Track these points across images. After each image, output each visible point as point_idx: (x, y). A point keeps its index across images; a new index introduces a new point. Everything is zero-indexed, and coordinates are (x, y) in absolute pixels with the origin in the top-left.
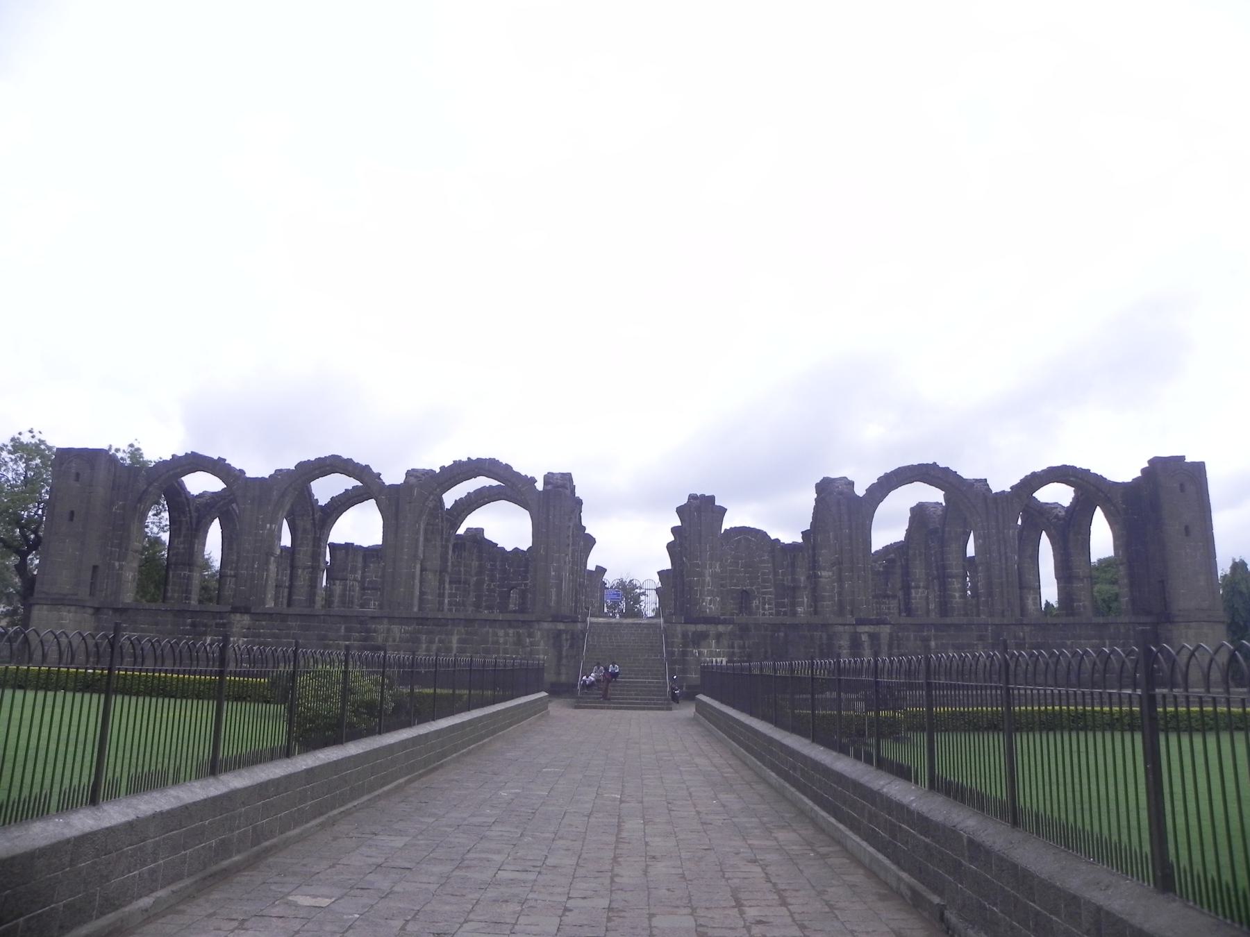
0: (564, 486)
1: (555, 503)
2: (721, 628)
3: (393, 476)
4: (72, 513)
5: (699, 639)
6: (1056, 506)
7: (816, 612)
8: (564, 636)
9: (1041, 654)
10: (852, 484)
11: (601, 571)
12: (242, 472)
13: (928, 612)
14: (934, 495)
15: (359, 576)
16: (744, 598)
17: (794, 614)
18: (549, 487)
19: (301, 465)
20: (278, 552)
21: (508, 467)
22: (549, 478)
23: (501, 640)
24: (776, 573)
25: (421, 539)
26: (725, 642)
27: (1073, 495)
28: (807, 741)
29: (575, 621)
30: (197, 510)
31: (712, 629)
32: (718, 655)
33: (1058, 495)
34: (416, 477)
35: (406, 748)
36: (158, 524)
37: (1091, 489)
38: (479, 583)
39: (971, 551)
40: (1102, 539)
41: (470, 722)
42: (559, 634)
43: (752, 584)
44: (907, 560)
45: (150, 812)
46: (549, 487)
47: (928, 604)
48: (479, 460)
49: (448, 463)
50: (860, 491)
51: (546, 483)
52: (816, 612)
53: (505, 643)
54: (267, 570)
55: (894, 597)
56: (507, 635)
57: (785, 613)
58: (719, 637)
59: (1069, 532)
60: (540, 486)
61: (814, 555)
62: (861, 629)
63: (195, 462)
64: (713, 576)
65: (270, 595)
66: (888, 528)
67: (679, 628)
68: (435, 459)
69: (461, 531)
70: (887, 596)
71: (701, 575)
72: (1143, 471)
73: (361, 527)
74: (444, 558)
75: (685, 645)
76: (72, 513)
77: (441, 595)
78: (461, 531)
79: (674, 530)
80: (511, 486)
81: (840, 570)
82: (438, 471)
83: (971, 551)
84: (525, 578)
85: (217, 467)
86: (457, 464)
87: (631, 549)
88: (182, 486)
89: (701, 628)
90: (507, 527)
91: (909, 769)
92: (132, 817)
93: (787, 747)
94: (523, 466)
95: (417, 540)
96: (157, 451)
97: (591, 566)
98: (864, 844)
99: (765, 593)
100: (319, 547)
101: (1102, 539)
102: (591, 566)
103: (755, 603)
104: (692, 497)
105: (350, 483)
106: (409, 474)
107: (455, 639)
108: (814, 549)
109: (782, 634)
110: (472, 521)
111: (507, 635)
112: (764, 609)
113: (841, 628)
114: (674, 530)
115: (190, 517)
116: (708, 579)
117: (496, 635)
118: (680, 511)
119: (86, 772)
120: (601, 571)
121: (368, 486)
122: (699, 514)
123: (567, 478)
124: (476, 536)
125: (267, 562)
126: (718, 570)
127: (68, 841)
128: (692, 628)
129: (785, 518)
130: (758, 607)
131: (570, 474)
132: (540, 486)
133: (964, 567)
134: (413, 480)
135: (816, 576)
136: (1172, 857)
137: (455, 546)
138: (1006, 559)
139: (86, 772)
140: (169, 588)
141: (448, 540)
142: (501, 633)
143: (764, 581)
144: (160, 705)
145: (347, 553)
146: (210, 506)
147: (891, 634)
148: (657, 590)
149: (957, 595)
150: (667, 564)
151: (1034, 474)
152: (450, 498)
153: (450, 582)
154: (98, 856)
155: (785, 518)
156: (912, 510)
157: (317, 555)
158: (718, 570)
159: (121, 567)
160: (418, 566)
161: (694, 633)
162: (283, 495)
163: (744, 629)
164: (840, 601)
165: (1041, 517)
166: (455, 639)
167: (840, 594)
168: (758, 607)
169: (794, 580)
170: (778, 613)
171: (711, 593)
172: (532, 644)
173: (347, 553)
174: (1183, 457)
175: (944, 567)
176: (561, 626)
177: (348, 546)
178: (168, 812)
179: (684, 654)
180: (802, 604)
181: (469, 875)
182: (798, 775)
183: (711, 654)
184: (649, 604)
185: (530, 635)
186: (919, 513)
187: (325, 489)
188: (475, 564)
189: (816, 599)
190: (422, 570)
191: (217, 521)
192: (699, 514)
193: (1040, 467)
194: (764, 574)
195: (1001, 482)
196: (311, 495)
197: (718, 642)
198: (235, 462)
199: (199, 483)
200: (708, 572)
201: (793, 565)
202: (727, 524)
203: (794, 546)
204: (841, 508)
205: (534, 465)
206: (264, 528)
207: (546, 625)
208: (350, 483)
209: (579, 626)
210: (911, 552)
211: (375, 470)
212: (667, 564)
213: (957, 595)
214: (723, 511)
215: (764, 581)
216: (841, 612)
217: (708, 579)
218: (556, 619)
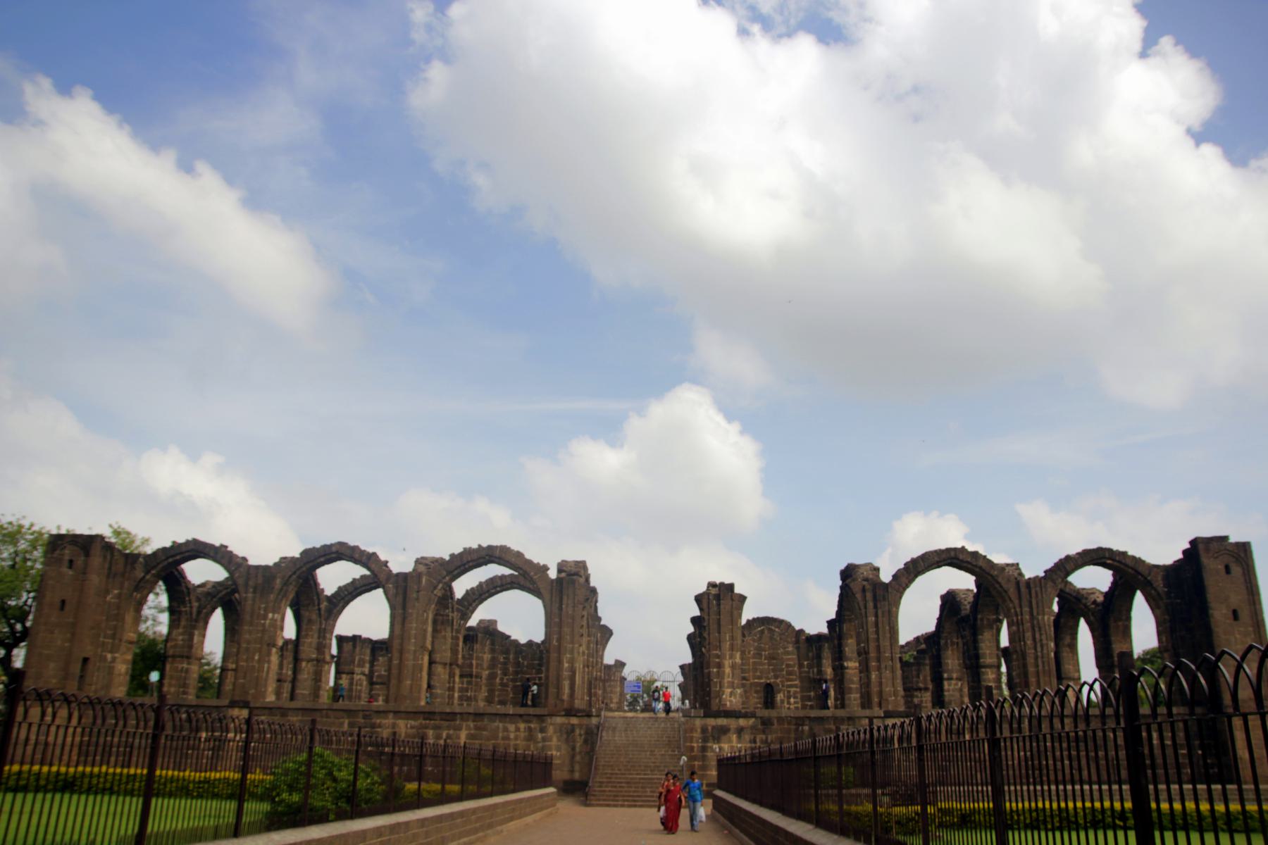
1: (569, 592)
2: (742, 722)
3: (401, 563)
4: (63, 602)
5: (722, 731)
6: (1093, 591)
8: (577, 731)
10: (877, 570)
11: (620, 665)
14: (964, 582)
16: (769, 692)
18: (563, 575)
22: (561, 567)
23: (512, 736)
24: (801, 666)
25: (430, 629)
26: (747, 737)
33: (1095, 580)
35: (381, 836)
36: (156, 614)
37: (1129, 573)
38: (492, 677)
40: (1144, 630)
42: (572, 729)
43: (776, 677)
44: (939, 650)
46: (563, 575)
48: (325, 547)
50: (886, 577)
51: (560, 571)
54: (269, 662)
56: (518, 729)
58: (740, 731)
59: (1109, 617)
60: (553, 574)
63: (196, 550)
65: (271, 687)
66: (917, 614)
68: (444, 549)
72: (1185, 552)
73: (368, 618)
75: (705, 740)
76: (63, 602)
77: (451, 689)
79: (695, 621)
80: (525, 576)
82: (447, 558)
84: (539, 672)
85: (219, 554)
86: (467, 551)
87: (649, 641)
88: (182, 575)
89: (722, 721)
90: (520, 617)
94: (535, 554)
96: (154, 535)
101: (1144, 630)
105: (357, 571)
108: (840, 638)
109: (806, 728)
111: (518, 729)
112: (789, 703)
114: (695, 621)
115: (189, 607)
117: (506, 730)
118: (699, 599)
120: (620, 665)
121: (376, 575)
122: (718, 602)
123: (582, 565)
124: (489, 629)
125: (269, 654)
128: (711, 722)
129: (814, 611)
130: (782, 701)
132: (553, 574)
134: (422, 568)
135: (842, 668)
142: (512, 727)
145: (354, 647)
146: (224, 597)
151: (1068, 558)
152: (462, 586)
153: (461, 676)
156: (943, 598)
160: (426, 658)
161: (713, 727)
165: (1074, 604)
169: (820, 672)
170: (804, 707)
171: (732, 685)
172: (544, 739)
174: (1225, 538)
175: (977, 657)
176: (574, 721)
179: (704, 749)
185: (542, 730)
186: (950, 601)
187: (332, 578)
188: (487, 657)
190: (431, 663)
192: (718, 602)
193: (1074, 549)
194: (788, 666)
195: (1033, 569)
196: (316, 584)
197: (739, 737)
198: (238, 549)
199: (200, 572)
200: (727, 663)
202: (748, 614)
203: (819, 637)
204: (866, 596)
205: (548, 555)
206: (265, 617)
207: (559, 720)
208: (357, 571)
209: (594, 721)
210: (942, 642)
214: (743, 599)
215: (790, 673)
217: (728, 670)
218: (570, 712)
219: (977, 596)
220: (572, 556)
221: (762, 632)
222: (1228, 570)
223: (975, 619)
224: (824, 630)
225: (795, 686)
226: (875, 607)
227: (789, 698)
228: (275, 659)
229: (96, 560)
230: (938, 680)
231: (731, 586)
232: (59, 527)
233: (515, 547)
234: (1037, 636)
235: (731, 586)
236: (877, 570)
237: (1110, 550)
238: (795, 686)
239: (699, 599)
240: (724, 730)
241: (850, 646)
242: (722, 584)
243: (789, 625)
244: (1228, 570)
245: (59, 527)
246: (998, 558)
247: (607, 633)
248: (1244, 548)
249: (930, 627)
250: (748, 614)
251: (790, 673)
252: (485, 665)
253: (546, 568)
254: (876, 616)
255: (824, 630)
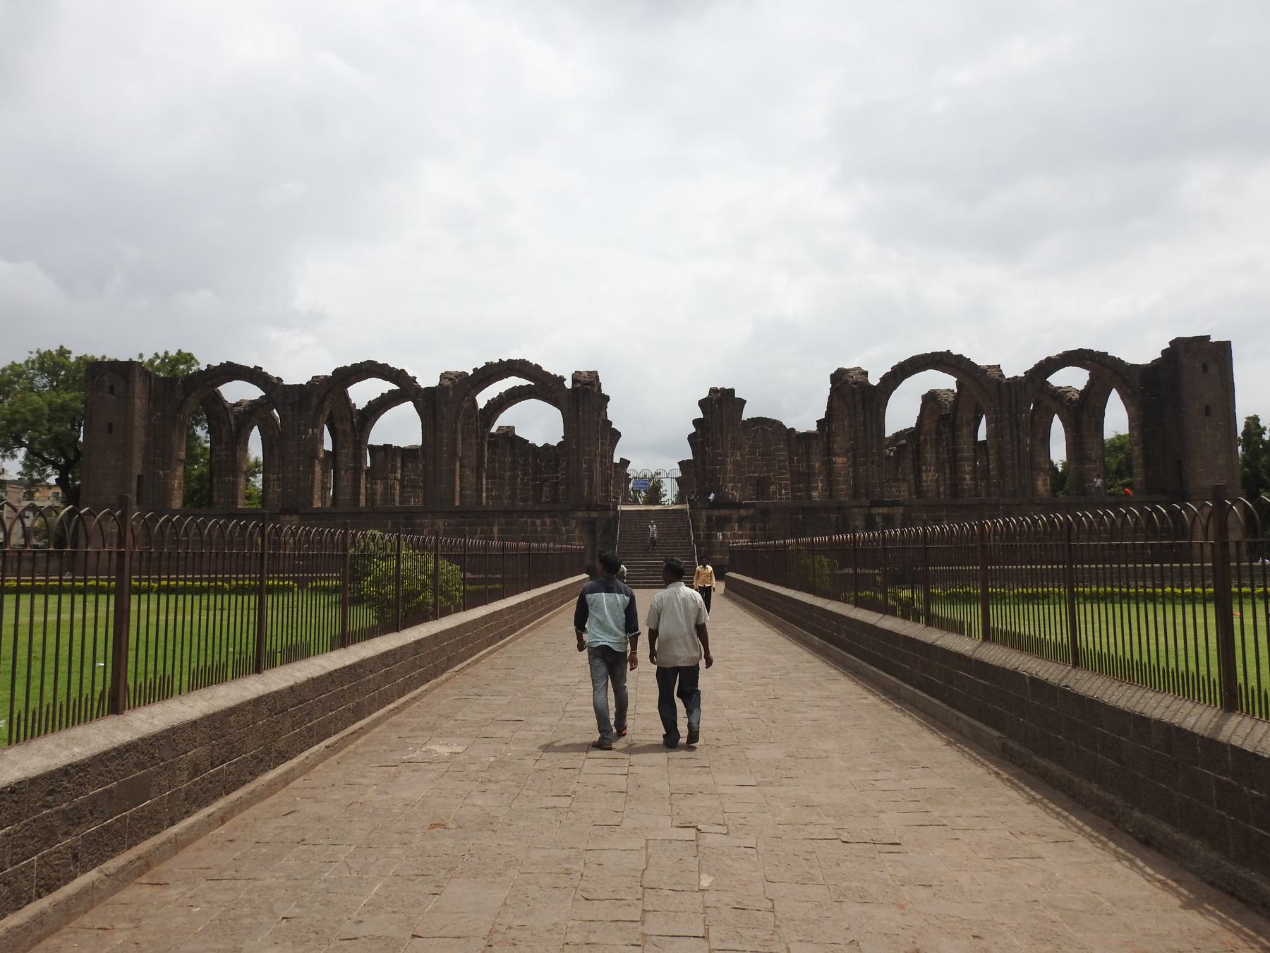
0: (591, 383)
1: (582, 400)
2: (743, 512)
3: (428, 379)
4: (110, 426)
5: (722, 523)
7: (831, 496)
9: (1129, 511)
10: (866, 373)
11: (625, 463)
12: (279, 379)
13: (938, 493)
14: (945, 382)
15: (399, 476)
16: (761, 486)
17: (810, 497)
19: (338, 372)
20: (322, 455)
21: (538, 367)
22: (576, 377)
24: (791, 461)
25: (459, 437)
27: (1088, 378)
28: (851, 606)
29: (607, 509)
30: (236, 417)
31: (735, 514)
32: (741, 537)
33: (1073, 379)
34: (450, 379)
39: (982, 434)
40: (1116, 419)
41: (532, 601)
45: (305, 679)
47: (938, 486)
48: (354, 365)
49: (480, 365)
50: (874, 380)
51: (575, 381)
52: (831, 496)
53: (543, 531)
55: (905, 480)
56: (544, 523)
57: (801, 497)
58: (741, 520)
59: (1083, 413)
60: (568, 384)
61: (829, 442)
62: (875, 511)
63: (232, 372)
64: (736, 463)
66: (902, 412)
67: (704, 513)
68: (468, 365)
69: (494, 430)
70: (897, 480)
71: (723, 463)
72: (1164, 352)
73: (401, 428)
74: (480, 456)
75: (709, 528)
76: (110, 426)
77: (480, 490)
78: (494, 430)
79: (696, 422)
80: (542, 385)
81: (854, 456)
82: (471, 372)
83: (982, 434)
85: (254, 375)
86: (489, 366)
87: (653, 439)
88: (219, 397)
89: (724, 512)
90: (539, 424)
91: (962, 623)
92: (291, 683)
93: (830, 612)
95: (455, 439)
97: (616, 460)
98: (918, 691)
99: (782, 479)
100: (360, 449)
101: (1116, 419)
102: (616, 460)
103: (773, 488)
104: (713, 391)
106: (444, 376)
107: (495, 529)
108: (829, 435)
110: (505, 419)
111: (544, 523)
113: (856, 510)
114: (696, 422)
115: (231, 425)
116: (729, 467)
117: (534, 524)
118: (702, 404)
119: (250, 646)
120: (625, 463)
121: (405, 387)
125: (313, 466)
126: (738, 458)
127: (249, 702)
129: (804, 410)
130: (775, 493)
131: (596, 372)
132: (568, 384)
133: (975, 451)
134: (447, 383)
135: (830, 462)
136: (1240, 679)
137: (489, 443)
138: (1019, 443)
139: (250, 646)
140: (215, 493)
141: (483, 438)
142: (538, 522)
143: (781, 468)
144: (172, 605)
145: (386, 455)
146: (251, 413)
147: (903, 515)
148: (677, 479)
149: (968, 477)
150: (688, 455)
151: (1049, 359)
152: (483, 399)
154: (270, 715)
155: (804, 410)
157: (359, 458)
158: (738, 458)
159: (166, 476)
160: (458, 464)
161: (717, 518)
162: (322, 401)
163: (765, 512)
164: (855, 485)
166: (495, 529)
167: (855, 478)
168: (775, 493)
169: (809, 466)
170: (794, 497)
171: (732, 480)
172: (568, 531)
173: (386, 455)
175: (955, 451)
176: (594, 515)
177: (387, 448)
178: (318, 678)
179: (709, 536)
180: (816, 489)
181: (576, 723)
182: (843, 636)
183: (735, 536)
184: (670, 490)
186: (930, 399)
187: (362, 393)
188: (509, 459)
189: (830, 482)
191: (256, 428)
193: (1055, 352)
194: (779, 461)
195: (1015, 367)
197: (740, 528)
198: (272, 370)
199: (237, 392)
201: (808, 453)
202: (747, 414)
203: (808, 435)
204: (855, 397)
205: (562, 366)
206: (306, 432)
207: (580, 514)
209: (611, 513)
210: (922, 438)
211: (411, 374)
212: (688, 455)
213: (968, 477)
214: (742, 402)
216: (856, 494)
217: (729, 467)
219: (957, 396)
220: (584, 368)
221: (756, 431)
222: (1205, 368)
223: (955, 418)
224: (814, 428)
225: (786, 479)
226: (864, 408)
227: (780, 490)
228: (318, 469)
229: (138, 386)
230: (918, 472)
231: (732, 391)
232: (141, 356)
233: (533, 361)
234: (1015, 432)
235: (732, 391)
236: (866, 373)
237: (1090, 351)
238: (786, 479)
239: (702, 404)
240: (728, 520)
241: (840, 443)
242: (723, 389)
243: (780, 425)
244: (1205, 368)
245: (141, 356)
246: (981, 360)
247: (616, 435)
248: (1225, 347)
249: (912, 423)
250: (747, 414)
251: (781, 468)
252: (508, 467)
253: (562, 379)
254: (865, 417)
255: (814, 428)
